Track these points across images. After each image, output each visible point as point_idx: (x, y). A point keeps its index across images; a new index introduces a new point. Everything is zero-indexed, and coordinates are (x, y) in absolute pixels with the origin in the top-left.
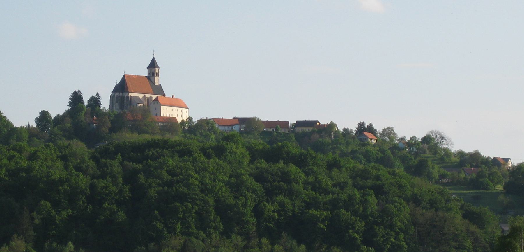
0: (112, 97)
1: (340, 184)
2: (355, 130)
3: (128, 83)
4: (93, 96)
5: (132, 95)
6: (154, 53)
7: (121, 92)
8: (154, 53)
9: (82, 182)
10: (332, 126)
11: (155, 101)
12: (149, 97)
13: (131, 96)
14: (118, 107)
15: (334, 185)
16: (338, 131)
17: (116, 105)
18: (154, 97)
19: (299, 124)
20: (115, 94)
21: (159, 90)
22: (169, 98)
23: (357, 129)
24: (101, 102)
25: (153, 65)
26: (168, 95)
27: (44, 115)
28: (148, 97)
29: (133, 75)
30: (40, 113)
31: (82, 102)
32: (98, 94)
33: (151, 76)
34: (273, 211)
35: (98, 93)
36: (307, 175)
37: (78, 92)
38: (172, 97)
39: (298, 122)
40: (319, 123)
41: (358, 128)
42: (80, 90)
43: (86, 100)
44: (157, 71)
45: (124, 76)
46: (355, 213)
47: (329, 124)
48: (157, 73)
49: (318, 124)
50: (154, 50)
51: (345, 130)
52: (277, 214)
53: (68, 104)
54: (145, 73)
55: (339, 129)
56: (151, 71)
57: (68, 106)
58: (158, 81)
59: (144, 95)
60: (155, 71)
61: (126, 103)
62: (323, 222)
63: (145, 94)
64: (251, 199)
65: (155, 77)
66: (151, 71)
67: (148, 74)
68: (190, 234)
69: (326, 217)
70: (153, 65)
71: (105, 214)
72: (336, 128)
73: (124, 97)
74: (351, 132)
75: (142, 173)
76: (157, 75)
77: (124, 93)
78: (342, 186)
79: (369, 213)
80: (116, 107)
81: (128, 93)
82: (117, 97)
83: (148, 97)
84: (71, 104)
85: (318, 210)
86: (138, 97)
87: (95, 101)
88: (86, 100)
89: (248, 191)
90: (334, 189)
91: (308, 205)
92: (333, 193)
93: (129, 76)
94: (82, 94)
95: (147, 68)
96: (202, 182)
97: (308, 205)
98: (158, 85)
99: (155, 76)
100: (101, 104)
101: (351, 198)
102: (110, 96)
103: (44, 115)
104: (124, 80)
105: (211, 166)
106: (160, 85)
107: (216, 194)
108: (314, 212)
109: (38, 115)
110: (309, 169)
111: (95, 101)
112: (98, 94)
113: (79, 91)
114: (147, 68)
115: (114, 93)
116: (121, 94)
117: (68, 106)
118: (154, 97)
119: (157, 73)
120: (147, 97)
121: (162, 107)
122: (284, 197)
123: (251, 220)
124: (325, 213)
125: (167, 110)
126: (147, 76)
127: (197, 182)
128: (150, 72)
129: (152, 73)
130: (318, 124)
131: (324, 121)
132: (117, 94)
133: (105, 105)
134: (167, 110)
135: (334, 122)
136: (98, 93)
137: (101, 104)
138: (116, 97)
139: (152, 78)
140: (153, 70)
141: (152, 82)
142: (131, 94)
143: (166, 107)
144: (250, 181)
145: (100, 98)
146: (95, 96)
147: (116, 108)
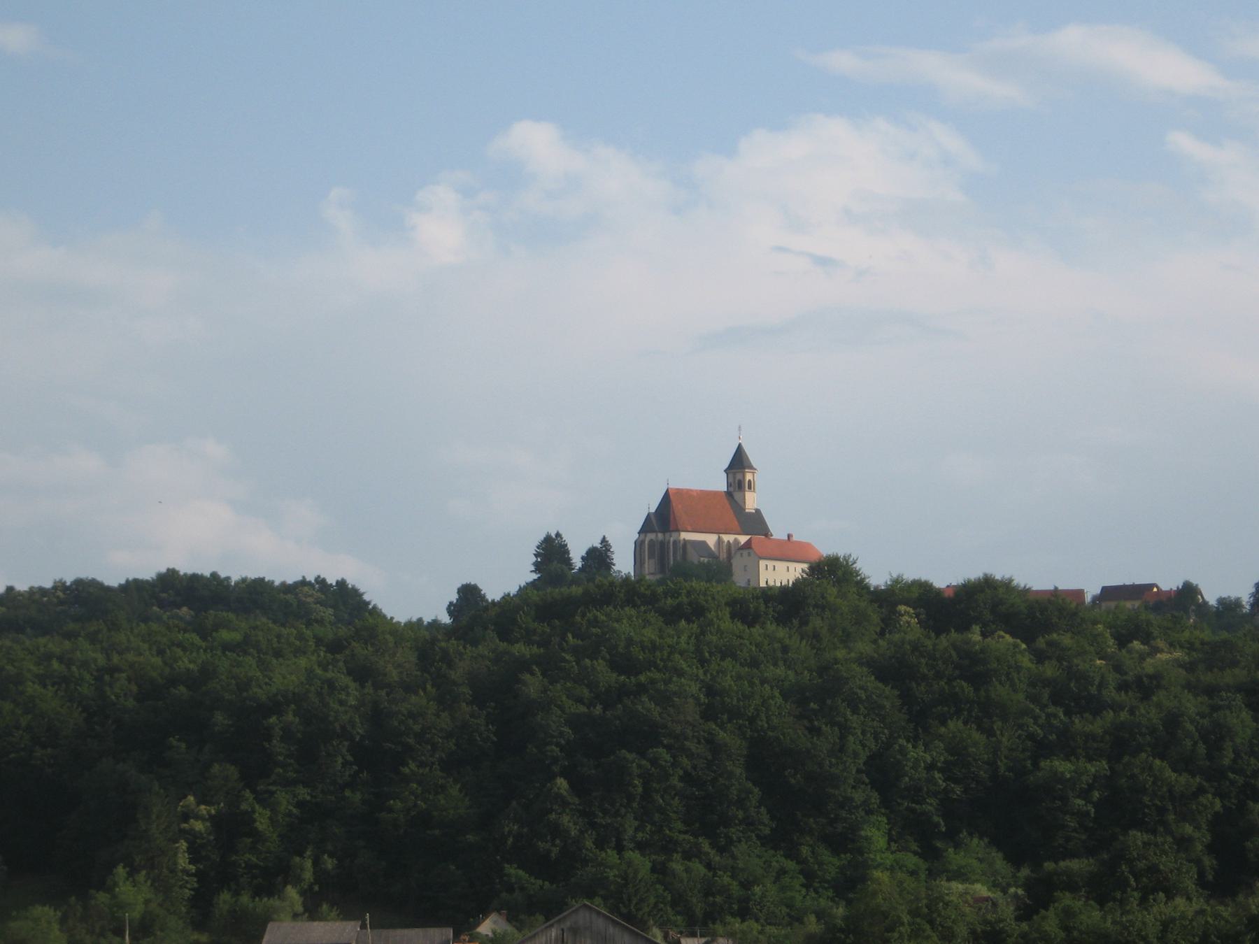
0: (639, 545)
1: (1139, 680)
2: (1248, 600)
3: (677, 507)
4: (594, 546)
5: (686, 539)
6: (740, 434)
7: (660, 532)
8: (740, 434)
9: (224, 667)
10: (1188, 592)
11: (742, 549)
12: (731, 542)
13: (684, 539)
14: (655, 569)
15: (1123, 687)
16: (1205, 603)
17: (648, 565)
18: (743, 539)
19: (1109, 593)
20: (646, 536)
21: (755, 524)
22: (779, 542)
23: (1251, 599)
24: (613, 559)
25: (739, 463)
26: (778, 531)
27: (469, 594)
28: (729, 541)
29: (691, 490)
30: (459, 591)
31: (567, 561)
32: (604, 541)
33: (734, 491)
34: (931, 767)
35: (604, 537)
36: (1040, 657)
37: (556, 536)
38: (786, 538)
39: (1104, 589)
40: (1157, 587)
41: (1255, 596)
42: (560, 532)
43: (577, 556)
44: (749, 477)
45: (667, 490)
46: (1185, 764)
47: (1180, 587)
48: (750, 481)
49: (1155, 590)
50: (740, 427)
51: (1221, 601)
52: (940, 775)
53: (533, 568)
54: (719, 484)
55: (1205, 597)
56: (734, 478)
57: (531, 571)
58: (751, 502)
59: (719, 537)
60: (744, 477)
61: (675, 553)
62: (1085, 794)
63: (721, 535)
64: (864, 733)
65: (746, 493)
66: (734, 478)
67: (729, 485)
68: (668, 847)
69: (1095, 777)
70: (739, 463)
71: (407, 793)
72: (1200, 597)
73: (669, 542)
74: (1237, 604)
75: (534, 667)
76: (750, 487)
77: (667, 535)
78: (1146, 687)
79: (1226, 762)
80: (649, 568)
81: (677, 533)
82: (652, 543)
83: (729, 541)
84: (538, 567)
85: (1072, 758)
86: (704, 543)
87: (599, 557)
88: (577, 556)
89: (855, 711)
90: (1122, 697)
91: (1042, 749)
92: (1117, 707)
93: (680, 493)
94: (565, 541)
95: (725, 471)
96: (710, 691)
97: (1042, 749)
98: (754, 511)
99: (744, 491)
100: (614, 565)
101: (1173, 721)
102: (635, 543)
103: (469, 594)
104: (667, 499)
105: (748, 644)
106: (758, 511)
107: (752, 720)
108: (1064, 767)
109: (454, 597)
110: (1050, 644)
111: (599, 557)
112: (604, 541)
113: (558, 535)
114: (725, 471)
115: (642, 536)
116: (660, 536)
117: (531, 571)
118: (743, 539)
119: (750, 481)
120: (726, 541)
121: (762, 563)
122: (965, 723)
123: (858, 796)
124: (1092, 768)
125: (774, 569)
126: (726, 490)
127: (694, 688)
128: (730, 480)
129: (737, 485)
130: (1155, 590)
131: (1169, 582)
132: (651, 536)
133: (623, 563)
134: (774, 569)
135: (1194, 581)
136: (604, 537)
137: (614, 565)
138: (649, 545)
139: (737, 496)
140: (739, 476)
141: (738, 508)
142: (685, 536)
143: (770, 564)
144: (863, 681)
145: (612, 550)
146: (599, 546)
147: (652, 572)
